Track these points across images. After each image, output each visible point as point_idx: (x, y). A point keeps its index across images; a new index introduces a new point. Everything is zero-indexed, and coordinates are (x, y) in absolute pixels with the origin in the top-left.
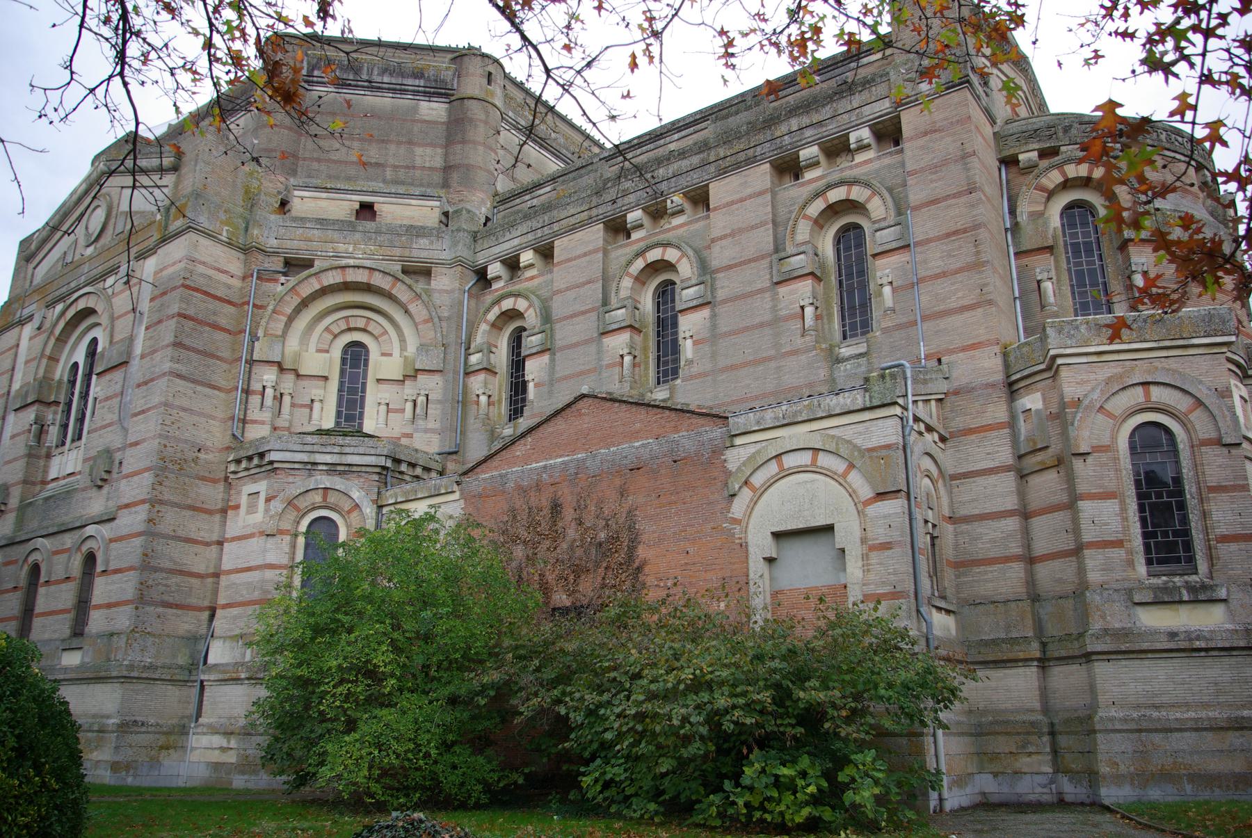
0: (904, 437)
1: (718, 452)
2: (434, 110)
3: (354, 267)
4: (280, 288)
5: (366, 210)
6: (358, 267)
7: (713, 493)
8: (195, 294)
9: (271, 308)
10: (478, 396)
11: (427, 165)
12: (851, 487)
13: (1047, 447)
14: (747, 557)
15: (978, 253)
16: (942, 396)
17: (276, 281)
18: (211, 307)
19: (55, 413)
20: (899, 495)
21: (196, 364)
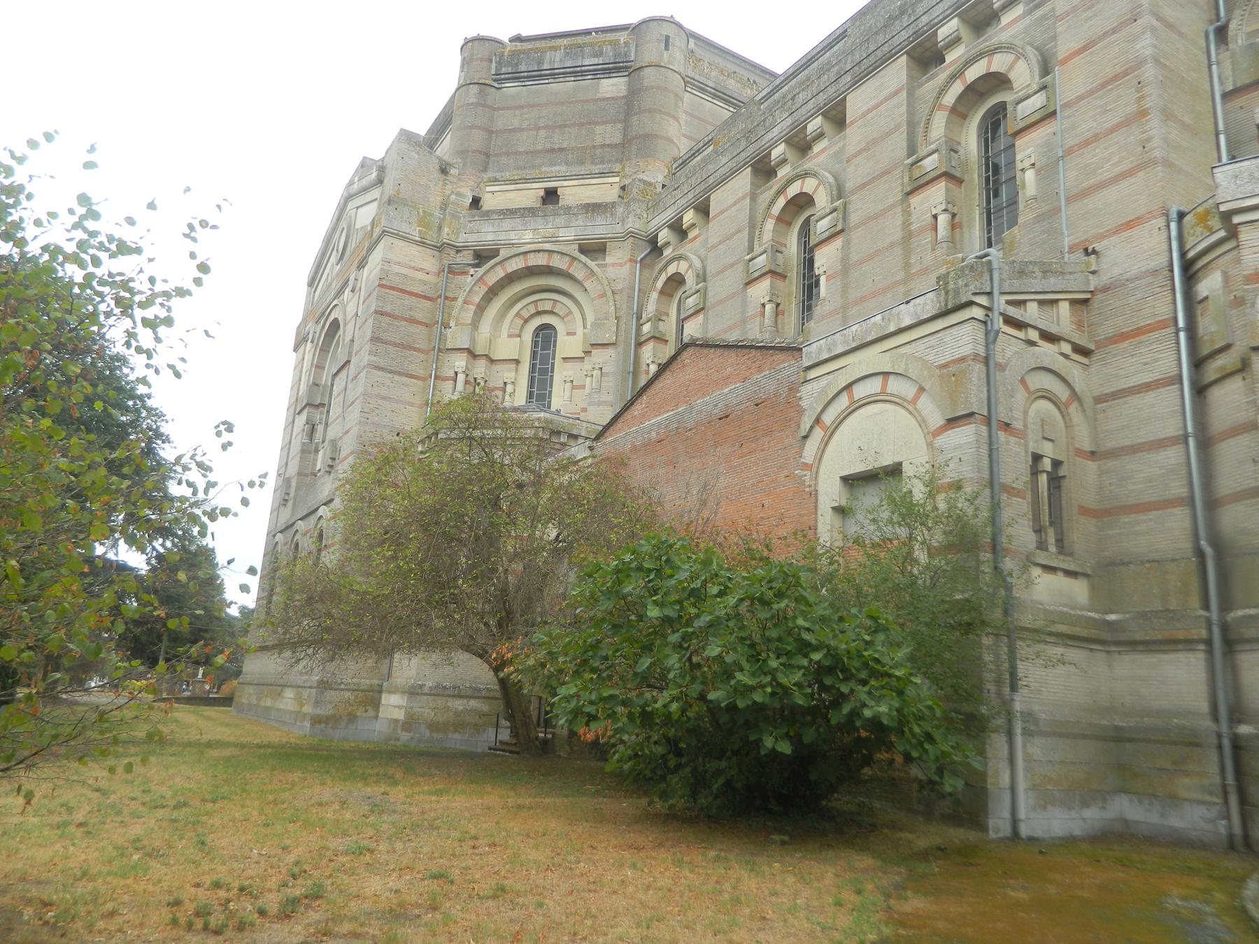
0: (987, 346)
1: (793, 389)
2: (613, 86)
3: (535, 251)
4: (469, 279)
5: (551, 196)
6: (539, 251)
7: (788, 437)
8: (391, 292)
9: (460, 300)
10: (648, 365)
11: (607, 142)
12: (920, 415)
13: (1227, 347)
14: (816, 507)
15: (1140, 99)
16: (1089, 296)
17: (466, 273)
18: (406, 302)
19: (322, 413)
20: (972, 419)
21: (394, 356)
